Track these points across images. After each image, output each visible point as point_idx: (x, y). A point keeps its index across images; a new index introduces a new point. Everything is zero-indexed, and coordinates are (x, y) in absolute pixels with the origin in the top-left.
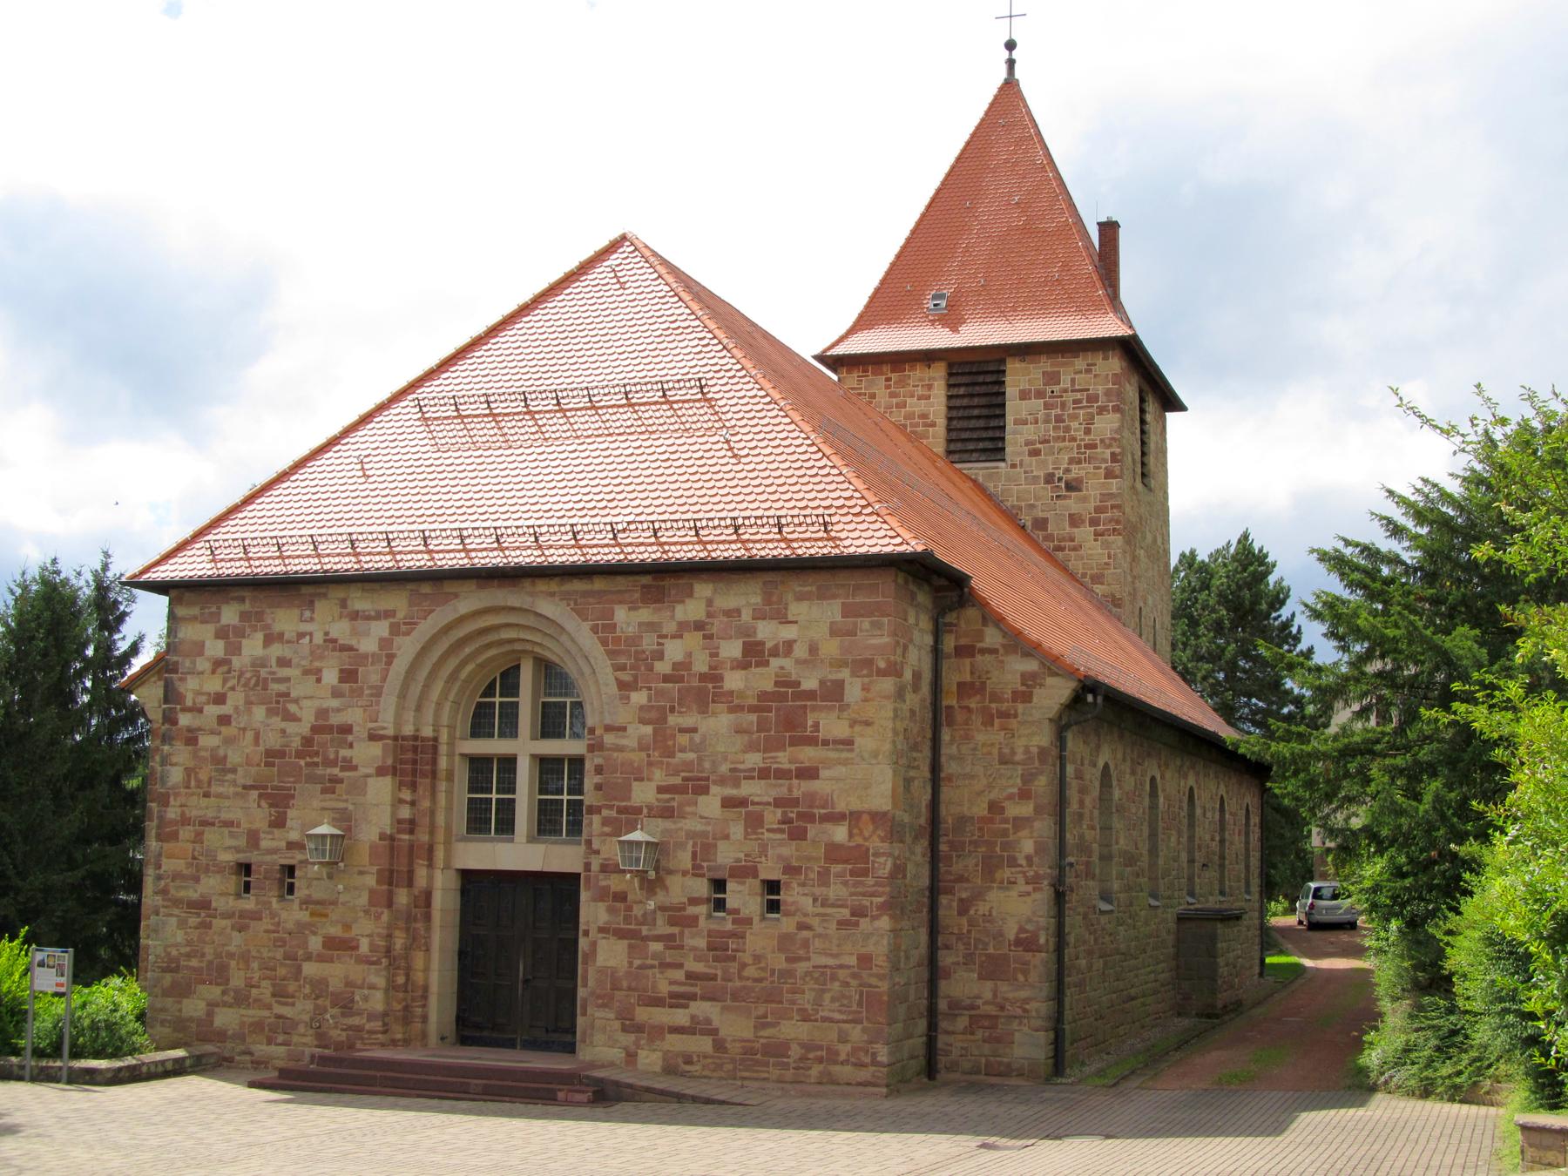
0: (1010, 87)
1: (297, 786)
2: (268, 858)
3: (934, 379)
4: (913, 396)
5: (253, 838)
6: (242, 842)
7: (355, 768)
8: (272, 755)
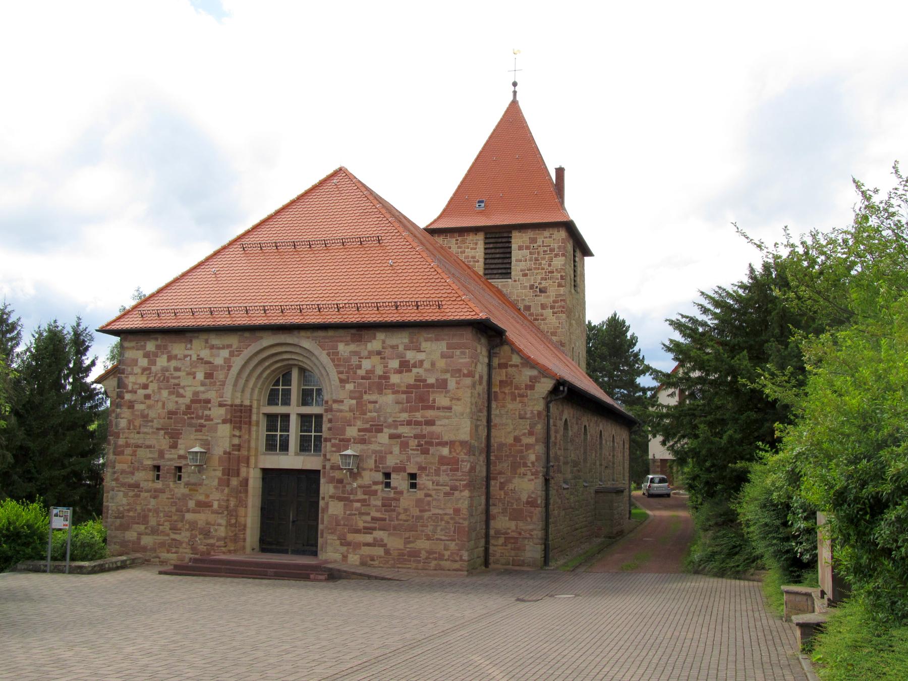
0: (514, 104)
5: (161, 454)
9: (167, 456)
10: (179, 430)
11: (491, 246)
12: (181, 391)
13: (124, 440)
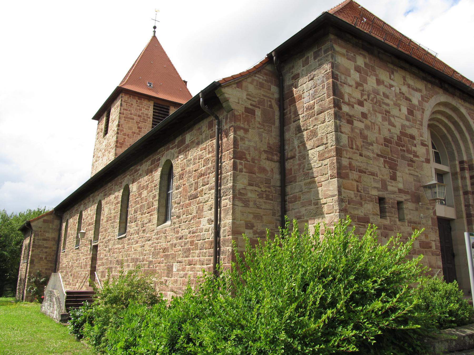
0: (154, 37)
1: (398, 160)
2: (392, 196)
3: (151, 105)
4: (144, 108)
5: (384, 186)
6: (379, 185)
7: (418, 157)
8: (387, 141)
9: (390, 188)
10: (395, 161)
11: (157, 111)
12: (392, 119)
13: (348, 160)
